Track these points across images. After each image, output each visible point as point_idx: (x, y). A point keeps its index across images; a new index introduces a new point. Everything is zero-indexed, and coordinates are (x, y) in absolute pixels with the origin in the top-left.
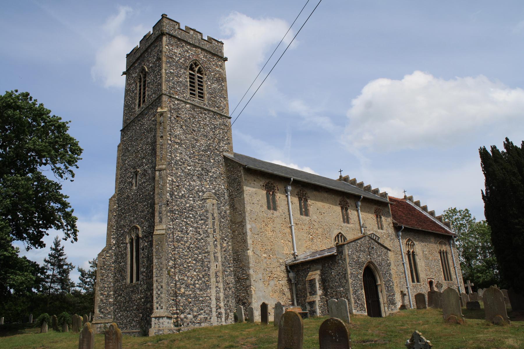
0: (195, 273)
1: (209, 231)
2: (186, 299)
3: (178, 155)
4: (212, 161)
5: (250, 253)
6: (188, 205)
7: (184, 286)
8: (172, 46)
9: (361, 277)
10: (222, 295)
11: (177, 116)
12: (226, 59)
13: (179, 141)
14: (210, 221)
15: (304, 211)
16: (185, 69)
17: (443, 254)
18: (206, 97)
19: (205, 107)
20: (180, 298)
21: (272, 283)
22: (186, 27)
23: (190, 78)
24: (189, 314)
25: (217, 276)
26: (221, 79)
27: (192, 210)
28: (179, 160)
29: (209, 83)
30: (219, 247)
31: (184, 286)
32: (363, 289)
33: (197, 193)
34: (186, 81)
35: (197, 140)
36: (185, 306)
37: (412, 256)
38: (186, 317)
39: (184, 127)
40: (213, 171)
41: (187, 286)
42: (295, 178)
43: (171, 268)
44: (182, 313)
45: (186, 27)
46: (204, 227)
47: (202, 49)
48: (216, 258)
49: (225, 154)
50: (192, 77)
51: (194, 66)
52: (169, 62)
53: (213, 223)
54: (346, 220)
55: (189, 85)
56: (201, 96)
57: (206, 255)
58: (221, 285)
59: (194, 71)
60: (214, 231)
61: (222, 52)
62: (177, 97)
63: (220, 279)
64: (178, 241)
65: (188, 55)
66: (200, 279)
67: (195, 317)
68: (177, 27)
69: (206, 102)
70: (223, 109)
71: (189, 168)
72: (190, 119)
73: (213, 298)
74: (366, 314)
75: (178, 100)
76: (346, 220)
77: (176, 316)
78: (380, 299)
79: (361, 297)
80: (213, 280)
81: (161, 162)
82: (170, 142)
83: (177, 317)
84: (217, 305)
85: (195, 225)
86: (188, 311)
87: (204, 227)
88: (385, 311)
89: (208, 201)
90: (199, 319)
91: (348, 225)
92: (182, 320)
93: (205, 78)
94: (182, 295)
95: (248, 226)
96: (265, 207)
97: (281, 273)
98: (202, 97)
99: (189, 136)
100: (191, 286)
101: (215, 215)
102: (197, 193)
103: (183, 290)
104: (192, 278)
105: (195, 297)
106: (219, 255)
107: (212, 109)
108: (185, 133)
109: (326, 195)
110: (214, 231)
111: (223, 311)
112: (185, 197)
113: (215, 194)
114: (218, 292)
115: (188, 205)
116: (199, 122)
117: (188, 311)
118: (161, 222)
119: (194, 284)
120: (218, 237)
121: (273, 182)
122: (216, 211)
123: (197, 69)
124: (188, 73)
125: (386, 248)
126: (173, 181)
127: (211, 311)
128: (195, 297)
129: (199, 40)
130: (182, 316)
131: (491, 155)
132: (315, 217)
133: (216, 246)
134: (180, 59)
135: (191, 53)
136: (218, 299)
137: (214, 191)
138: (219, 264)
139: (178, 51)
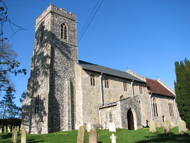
6: (58, 83)
7: (56, 115)
9: (126, 114)
15: (107, 86)
17: (171, 104)
19: (67, 43)
20: (54, 120)
24: (57, 126)
31: (56, 115)
34: (60, 32)
37: (155, 106)
38: (56, 127)
40: (70, 69)
42: (103, 72)
43: (51, 108)
44: (55, 126)
47: (67, 18)
54: (125, 89)
56: (65, 38)
57: (65, 103)
65: (61, 21)
71: (59, 68)
73: (67, 120)
74: (127, 128)
76: (125, 89)
77: (52, 127)
78: (75, 127)
79: (125, 122)
81: (76, 51)
83: (53, 128)
84: (69, 123)
88: (136, 127)
92: (54, 128)
96: (90, 84)
103: (55, 117)
107: (70, 43)
111: (71, 125)
115: (58, 83)
121: (94, 74)
127: (66, 125)
130: (55, 127)
131: (180, 64)
134: (58, 23)
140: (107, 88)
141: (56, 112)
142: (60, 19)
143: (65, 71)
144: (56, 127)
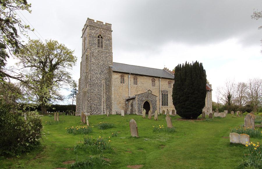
5: (113, 96)
8: (91, 30)
10: (105, 107)
12: (112, 31)
14: (102, 87)
21: (120, 105)
25: (104, 102)
26: (110, 39)
30: (105, 94)
35: (100, 62)
36: (94, 110)
39: (95, 58)
41: (95, 105)
48: (104, 97)
49: (109, 66)
58: (105, 105)
61: (111, 29)
62: (93, 48)
64: (92, 93)
66: (99, 103)
67: (96, 113)
68: (93, 22)
69: (104, 49)
72: (97, 55)
80: (102, 103)
89: (102, 81)
91: (154, 87)
93: (104, 40)
94: (93, 107)
95: (113, 89)
96: (120, 83)
97: (123, 102)
101: (104, 85)
103: (93, 106)
106: (105, 97)
108: (95, 60)
109: (146, 77)
113: (105, 78)
114: (104, 107)
116: (100, 56)
118: (86, 88)
119: (97, 104)
122: (104, 83)
123: (100, 37)
125: (156, 96)
129: (102, 25)
130: (93, 112)
132: (139, 85)
135: (99, 32)
136: (104, 108)
139: (93, 31)
142: (97, 31)
143: (101, 73)
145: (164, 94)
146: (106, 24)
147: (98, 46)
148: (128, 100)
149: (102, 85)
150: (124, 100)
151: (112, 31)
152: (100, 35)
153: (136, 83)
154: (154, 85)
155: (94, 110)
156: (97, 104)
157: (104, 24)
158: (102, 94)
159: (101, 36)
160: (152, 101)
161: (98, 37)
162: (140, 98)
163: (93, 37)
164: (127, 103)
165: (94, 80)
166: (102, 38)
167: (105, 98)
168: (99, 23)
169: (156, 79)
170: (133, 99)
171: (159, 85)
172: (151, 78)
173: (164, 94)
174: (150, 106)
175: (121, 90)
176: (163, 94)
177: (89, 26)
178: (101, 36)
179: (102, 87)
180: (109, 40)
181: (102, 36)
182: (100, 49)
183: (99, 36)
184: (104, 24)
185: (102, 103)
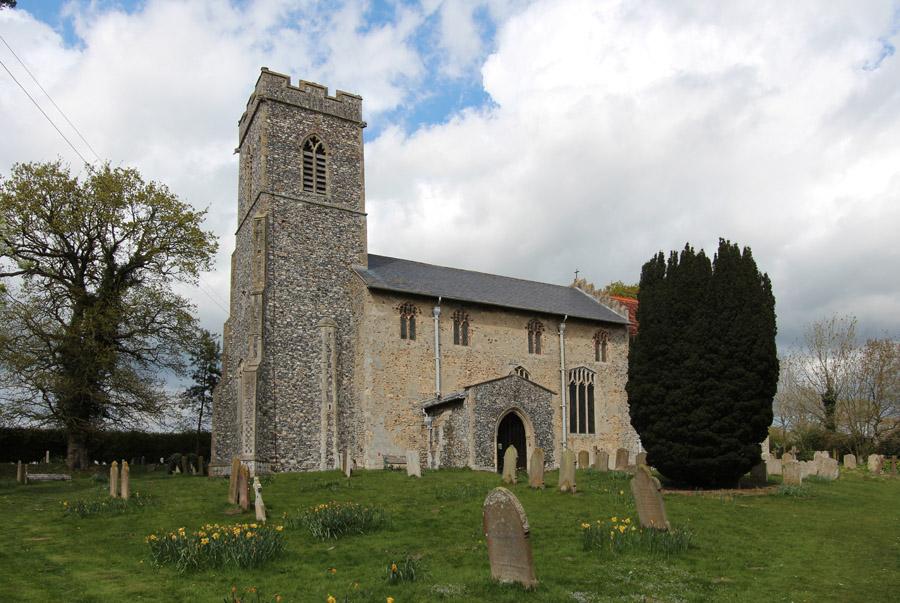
0: (302, 414)
1: (322, 365)
2: (289, 443)
3: (284, 273)
4: (334, 277)
11: (283, 221)
12: (364, 126)
13: (285, 255)
16: (298, 150)
18: (328, 188)
21: (399, 428)
22: (301, 81)
23: (305, 162)
25: (329, 417)
26: (355, 159)
27: (300, 341)
28: (285, 280)
29: (335, 167)
30: (334, 384)
31: (286, 428)
32: (496, 439)
33: (308, 320)
35: (312, 252)
38: (287, 462)
39: (293, 235)
41: (291, 428)
44: (283, 457)
45: (301, 81)
46: (316, 360)
49: (353, 266)
50: (307, 161)
51: (311, 143)
52: (272, 144)
53: (328, 357)
55: (302, 174)
56: (321, 187)
58: (334, 429)
59: (312, 151)
60: (329, 366)
61: (358, 115)
62: (283, 194)
63: (334, 421)
68: (284, 85)
70: (355, 203)
75: (285, 198)
82: (272, 257)
85: (305, 359)
86: (290, 455)
87: (316, 360)
90: (305, 464)
91: (538, 356)
94: (283, 439)
96: (398, 336)
98: (324, 189)
99: (300, 247)
100: (296, 429)
101: (332, 347)
102: (308, 320)
103: (284, 433)
104: (298, 419)
105: (301, 441)
106: (334, 394)
108: (294, 242)
110: (329, 366)
112: (291, 325)
113: (336, 319)
114: (329, 436)
115: (295, 335)
116: (316, 226)
117: (290, 455)
119: (300, 427)
120: (334, 372)
123: (315, 149)
124: (302, 156)
125: (548, 391)
126: (275, 306)
128: (301, 441)
130: (283, 461)
132: (478, 346)
133: (331, 383)
135: (307, 125)
136: (329, 444)
137: (333, 316)
138: (334, 404)
139: (285, 124)
140: (460, 347)
141: (289, 420)
142: (300, 122)
144: (287, 462)
145: (578, 383)
146: (341, 94)
147: (305, 186)
148: (433, 410)
149: (324, 347)
150: (417, 411)
151: (364, 126)
152: (314, 141)
153: (462, 338)
154: (535, 347)
155: (287, 451)
156: (300, 427)
157: (332, 94)
158: (322, 385)
159: (317, 145)
160: (533, 412)
161: (307, 148)
162: (486, 401)
163: (286, 147)
164: (427, 419)
165: (289, 324)
166: (320, 150)
167: (335, 399)
168: (309, 90)
169: (545, 322)
170: (456, 403)
171: (556, 349)
172: (525, 321)
173: (578, 383)
174: (528, 434)
175: (403, 369)
176: (572, 386)
177: (269, 102)
178: (317, 145)
179: (324, 354)
180: (350, 161)
181: (321, 145)
182: (313, 195)
183: (308, 142)
184: (332, 94)
185: (324, 422)
